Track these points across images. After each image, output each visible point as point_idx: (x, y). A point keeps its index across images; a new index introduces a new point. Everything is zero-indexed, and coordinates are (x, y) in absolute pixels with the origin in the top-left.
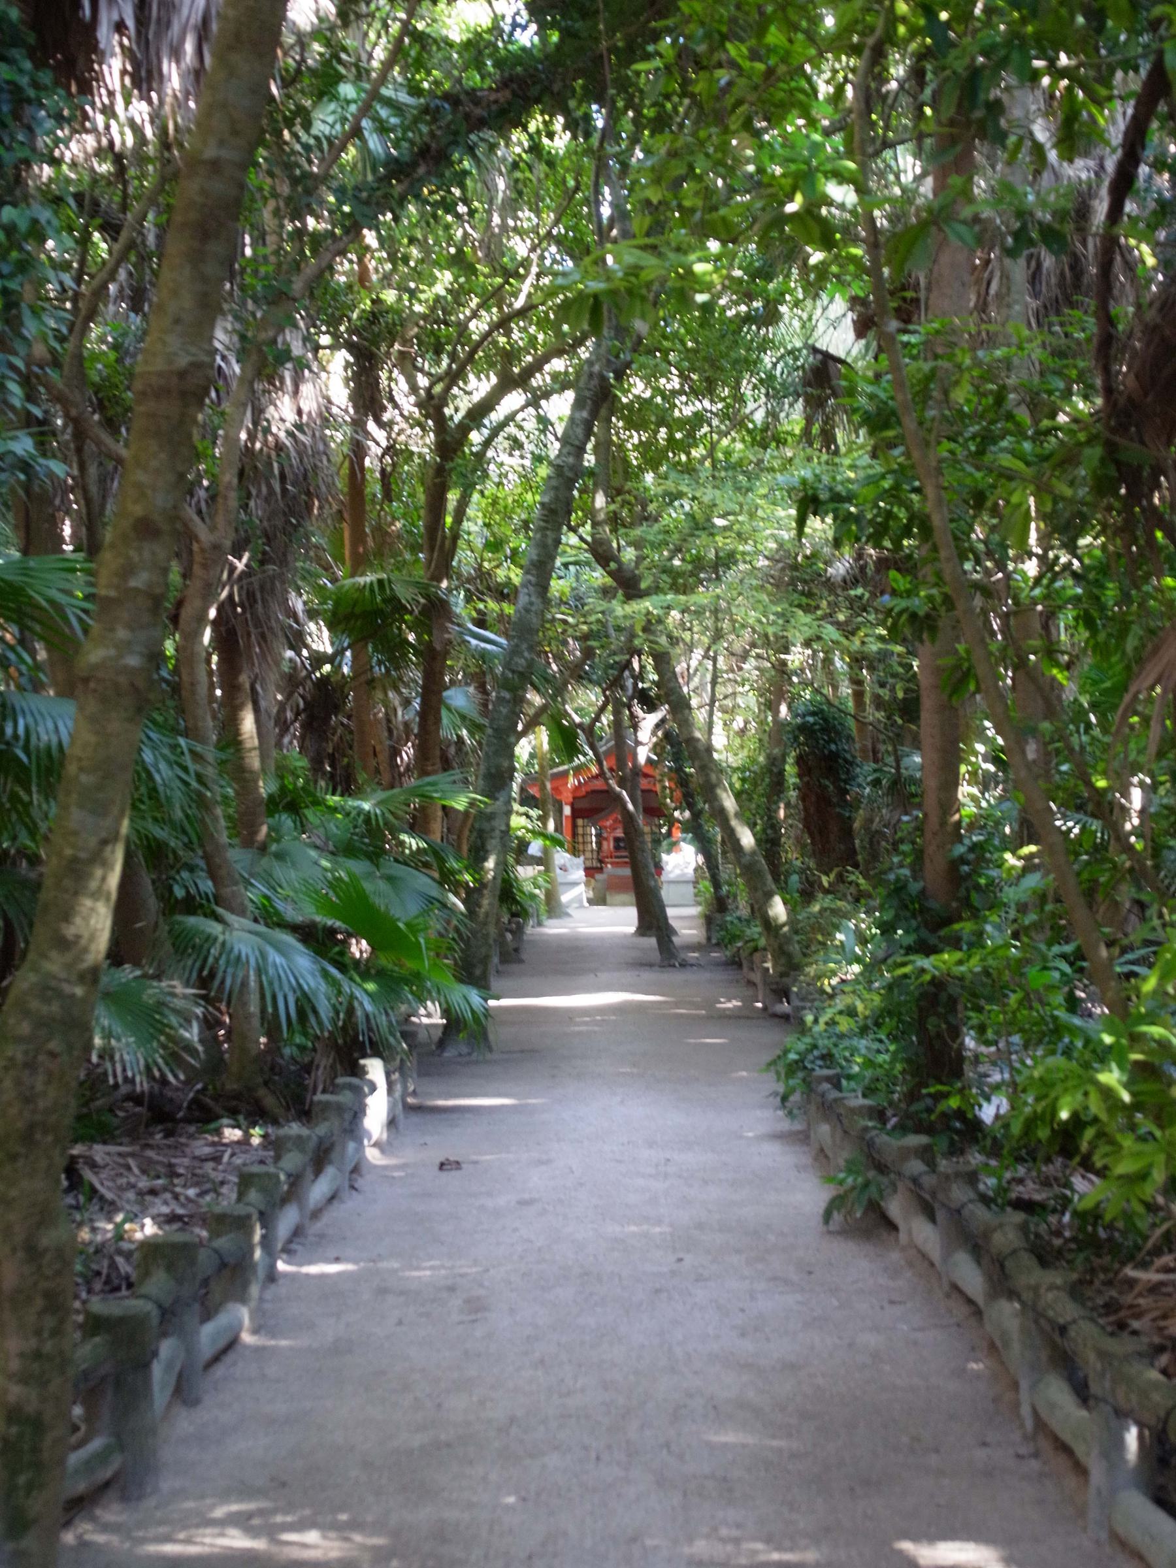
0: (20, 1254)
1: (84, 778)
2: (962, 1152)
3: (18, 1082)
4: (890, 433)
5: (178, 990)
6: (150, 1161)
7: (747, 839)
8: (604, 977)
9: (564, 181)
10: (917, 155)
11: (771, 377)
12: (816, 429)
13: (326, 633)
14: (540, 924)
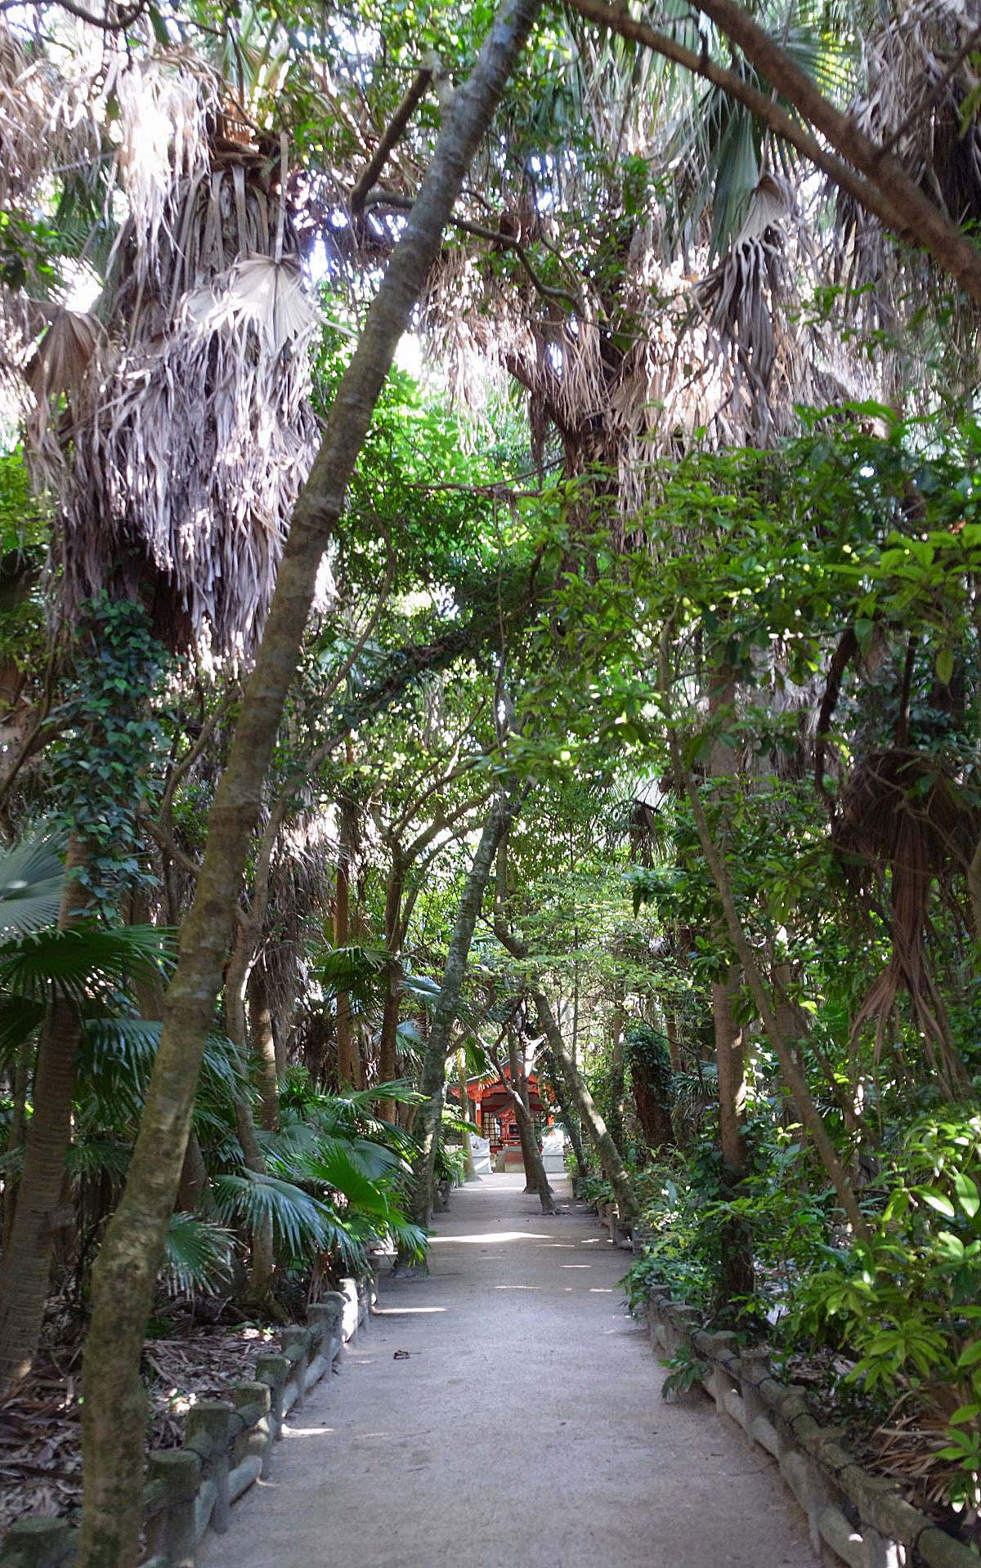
0: (109, 1414)
1: (167, 1075)
2: (757, 1345)
3: (113, 1288)
4: (694, 848)
5: (219, 1231)
6: (195, 1352)
7: (601, 1126)
8: (506, 1221)
9: (476, 699)
10: (699, 681)
11: (609, 819)
12: (638, 853)
13: (319, 990)
14: (460, 1185)
